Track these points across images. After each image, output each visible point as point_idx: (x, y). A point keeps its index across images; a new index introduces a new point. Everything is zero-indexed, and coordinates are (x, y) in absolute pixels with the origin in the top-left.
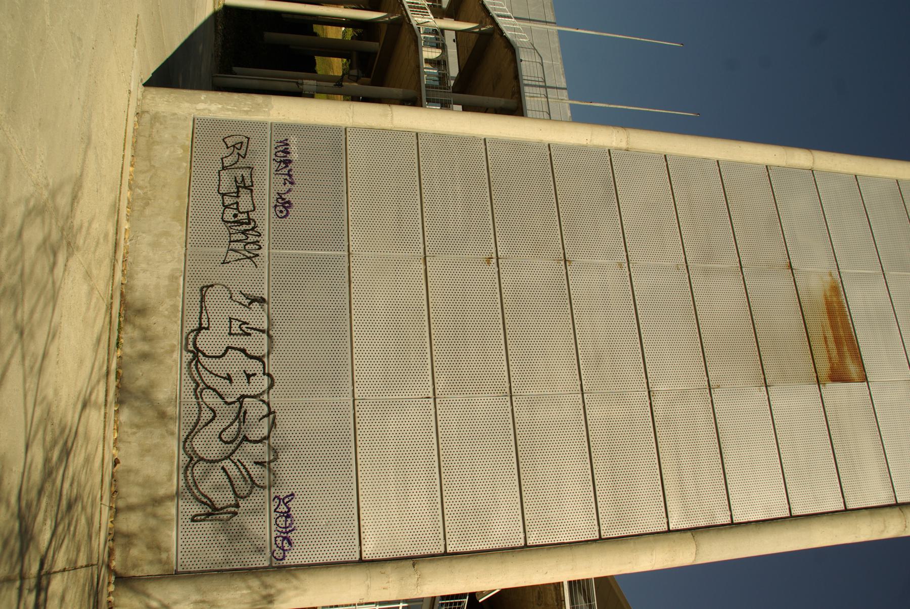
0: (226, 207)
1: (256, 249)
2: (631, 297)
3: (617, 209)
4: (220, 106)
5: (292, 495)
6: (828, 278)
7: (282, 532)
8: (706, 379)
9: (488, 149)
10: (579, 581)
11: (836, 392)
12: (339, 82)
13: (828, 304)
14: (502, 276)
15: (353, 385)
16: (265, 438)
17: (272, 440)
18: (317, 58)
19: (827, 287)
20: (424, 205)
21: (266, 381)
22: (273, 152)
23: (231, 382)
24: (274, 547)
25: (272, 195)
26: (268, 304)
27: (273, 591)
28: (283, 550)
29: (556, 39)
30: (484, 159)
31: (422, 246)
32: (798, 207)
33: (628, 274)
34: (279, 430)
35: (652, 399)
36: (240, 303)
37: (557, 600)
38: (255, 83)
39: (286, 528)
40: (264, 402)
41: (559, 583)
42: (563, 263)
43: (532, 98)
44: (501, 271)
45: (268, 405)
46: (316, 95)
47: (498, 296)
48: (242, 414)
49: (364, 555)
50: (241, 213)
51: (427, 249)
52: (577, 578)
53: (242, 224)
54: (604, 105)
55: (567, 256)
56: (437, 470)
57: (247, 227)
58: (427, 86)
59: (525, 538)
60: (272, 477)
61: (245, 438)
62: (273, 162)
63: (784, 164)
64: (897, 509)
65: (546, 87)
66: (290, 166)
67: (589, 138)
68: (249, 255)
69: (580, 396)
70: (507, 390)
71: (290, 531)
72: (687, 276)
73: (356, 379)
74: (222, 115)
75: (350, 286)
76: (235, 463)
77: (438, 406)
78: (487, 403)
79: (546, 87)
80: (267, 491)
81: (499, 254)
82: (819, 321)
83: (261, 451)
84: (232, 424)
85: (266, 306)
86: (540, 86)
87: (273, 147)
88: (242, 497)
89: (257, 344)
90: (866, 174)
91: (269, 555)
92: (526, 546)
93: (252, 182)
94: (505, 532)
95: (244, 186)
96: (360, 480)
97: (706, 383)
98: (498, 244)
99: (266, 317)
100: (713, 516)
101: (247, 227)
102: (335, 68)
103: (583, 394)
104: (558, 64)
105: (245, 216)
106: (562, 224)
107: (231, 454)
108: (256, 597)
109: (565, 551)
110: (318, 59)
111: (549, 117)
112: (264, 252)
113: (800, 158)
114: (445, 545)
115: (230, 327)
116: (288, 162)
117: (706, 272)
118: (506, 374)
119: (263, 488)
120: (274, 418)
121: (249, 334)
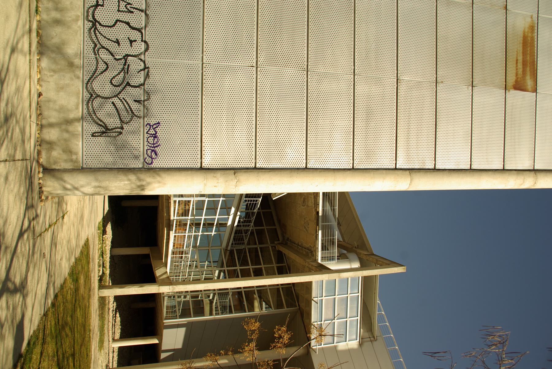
5: (159, 123)
6: (529, 20)
11: (515, 96)
13: (525, 38)
17: (146, 86)
19: (527, 25)
23: (119, 44)
24: (146, 156)
27: (144, 183)
28: (152, 158)
35: (399, 84)
39: (154, 144)
40: (141, 60)
45: (144, 62)
49: (203, 165)
60: (146, 111)
61: (128, 84)
64: (533, 172)
69: (352, 76)
70: (305, 67)
71: (156, 146)
72: (435, 4)
73: (205, 49)
77: (259, 73)
78: (292, 74)
80: (142, 120)
82: (516, 47)
83: (138, 93)
84: (119, 74)
89: (138, 20)
92: (306, 168)
103: (354, 75)
108: (134, 186)
114: (256, 163)
115: (119, 6)
119: (140, 117)
120: (148, 72)
121: (132, 12)
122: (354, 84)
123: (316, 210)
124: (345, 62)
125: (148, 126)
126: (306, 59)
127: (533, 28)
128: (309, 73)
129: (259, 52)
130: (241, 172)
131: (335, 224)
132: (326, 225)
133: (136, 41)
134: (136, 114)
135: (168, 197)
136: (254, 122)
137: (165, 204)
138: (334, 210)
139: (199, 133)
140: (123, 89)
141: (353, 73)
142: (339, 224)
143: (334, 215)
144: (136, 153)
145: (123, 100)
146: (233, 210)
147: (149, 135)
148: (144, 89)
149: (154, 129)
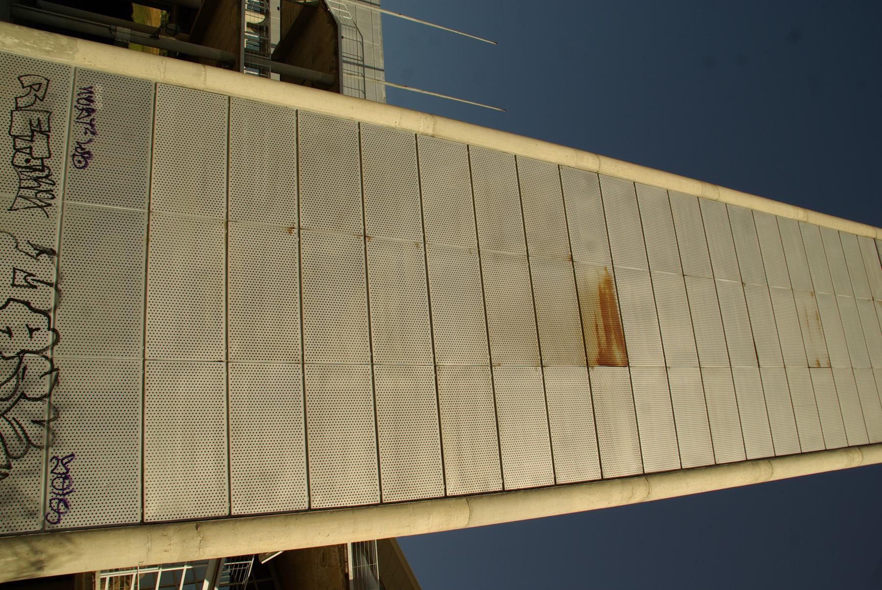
0: (18, 150)
1: (48, 199)
4: (17, 41)
5: (73, 455)
7: (58, 494)
8: (488, 357)
9: (299, 121)
10: (362, 542)
11: (602, 373)
12: (155, 34)
13: (602, 296)
14: (302, 246)
15: (144, 345)
16: (45, 396)
17: (53, 398)
18: (134, 5)
19: (602, 280)
20: (231, 170)
21: (50, 337)
22: (76, 98)
23: (11, 335)
24: (49, 510)
25: (71, 144)
26: (58, 256)
27: (43, 557)
28: (59, 513)
29: (379, 22)
30: (295, 130)
31: (225, 210)
33: (423, 254)
34: (61, 388)
36: (27, 254)
37: (340, 562)
38: (63, 22)
39: (63, 489)
40: (47, 358)
41: (343, 545)
42: (362, 238)
43: (349, 76)
44: (302, 241)
45: (51, 361)
46: (131, 45)
47: (297, 265)
48: (21, 370)
49: (146, 517)
50: (35, 159)
51: (230, 213)
52: (360, 540)
53: (35, 170)
54: (418, 91)
55: (367, 232)
56: (225, 433)
57: (41, 174)
58: (246, 50)
59: (309, 501)
60: (51, 437)
61: (23, 396)
62: (74, 109)
63: (574, 165)
64: (644, 478)
65: (364, 66)
66: (93, 115)
68: (40, 204)
69: (370, 367)
70: (300, 358)
71: (67, 493)
72: (478, 260)
73: (147, 339)
74: (19, 51)
75: (147, 245)
76: (10, 422)
77: (230, 370)
79: (364, 66)
80: (44, 451)
81: (301, 224)
82: (592, 310)
83: (40, 409)
84: (8, 380)
85: (56, 258)
86: (358, 65)
87: (76, 93)
88: (15, 458)
89: (44, 298)
90: (642, 181)
91: (41, 517)
92: (310, 509)
93: (49, 127)
94: (291, 496)
95: (39, 130)
96: (146, 441)
99: (55, 270)
101: (41, 174)
102: (153, 18)
104: (379, 45)
105: (39, 162)
107: (6, 412)
108: (24, 564)
109: (348, 515)
110: (136, 7)
111: (363, 96)
112: (58, 201)
113: (588, 161)
114: (230, 508)
115: (14, 278)
116: (90, 111)
117: (496, 257)
118: (299, 342)
119: (41, 448)
120: (57, 376)
121: (35, 287)
122: (373, 378)
123: (343, 570)
125: (54, 460)
127: (609, 283)
130: (207, 523)
133: (39, 329)
134: (35, 443)
135: (91, 575)
137: (84, 586)
138: (373, 568)
139: (139, 466)
140: (14, 404)
143: (376, 578)
144: (31, 506)
145: (13, 422)
147: (55, 476)
148: (50, 403)
149: (64, 465)
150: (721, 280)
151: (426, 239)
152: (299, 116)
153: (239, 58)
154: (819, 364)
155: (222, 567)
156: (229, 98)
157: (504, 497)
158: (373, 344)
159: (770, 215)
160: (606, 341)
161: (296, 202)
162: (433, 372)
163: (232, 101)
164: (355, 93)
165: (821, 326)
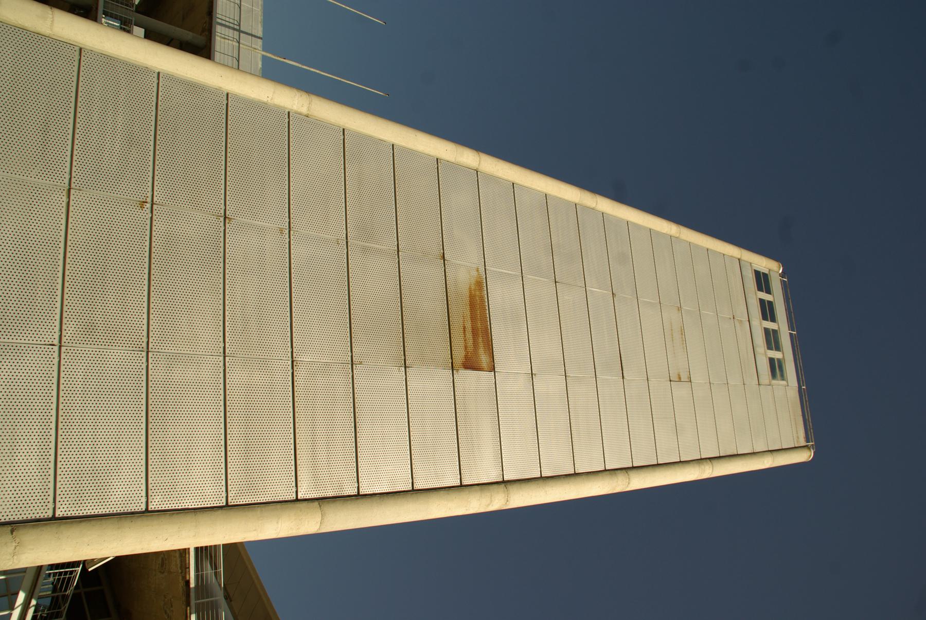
2: (287, 265)
3: (287, 173)
6: (475, 273)
8: (350, 354)
9: (161, 84)
10: (206, 547)
11: (467, 378)
13: (472, 297)
14: (154, 223)
19: (473, 281)
31: (67, 176)
32: (459, 200)
33: (287, 241)
35: (295, 368)
37: (181, 568)
41: (185, 549)
42: (222, 219)
43: (222, 40)
44: (154, 218)
51: (73, 180)
52: (204, 545)
55: (228, 213)
63: (453, 160)
64: (503, 485)
65: (240, 31)
67: (270, 96)
69: (221, 358)
70: (144, 345)
77: (63, 356)
78: (120, 357)
79: (240, 31)
82: (461, 311)
86: (234, 29)
92: (227, 505)
94: (125, 494)
97: (350, 359)
98: (156, 188)
100: (341, 488)
103: (225, 357)
104: (258, 10)
106: (228, 179)
111: (237, 66)
113: (468, 158)
117: (365, 250)
122: (225, 370)
123: (184, 577)
124: (209, 336)
126: (145, 333)
128: (150, 354)
129: (65, 321)
131: (220, 597)
132: (203, 603)
136: (53, 439)
141: (222, 354)
142: (227, 597)
143: (220, 585)
146: (22, 596)
150: (593, 289)
151: (292, 225)
152: (230, 100)
153: (97, 4)
154: (680, 378)
155: (43, 576)
156: (81, 49)
157: (359, 501)
158: (227, 334)
159: (645, 228)
160: (473, 344)
161: (151, 174)
162: (290, 368)
163: (83, 54)
164: (229, 61)
165: (684, 341)
